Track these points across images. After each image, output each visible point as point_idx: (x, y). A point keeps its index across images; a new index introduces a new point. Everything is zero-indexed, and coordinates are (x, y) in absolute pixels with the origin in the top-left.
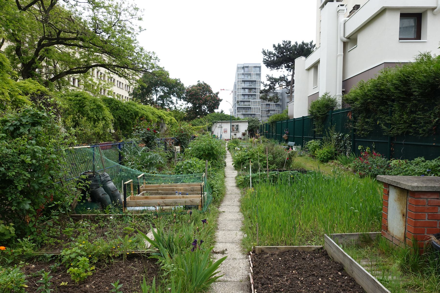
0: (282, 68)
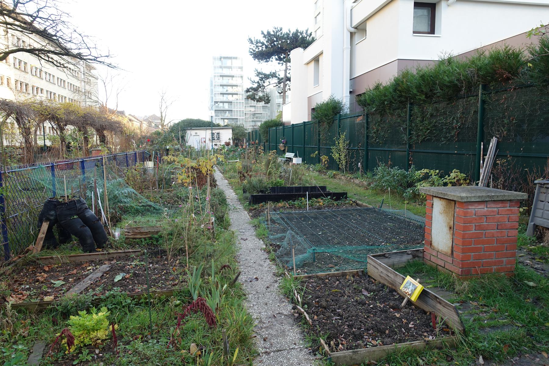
0: (272, 61)
